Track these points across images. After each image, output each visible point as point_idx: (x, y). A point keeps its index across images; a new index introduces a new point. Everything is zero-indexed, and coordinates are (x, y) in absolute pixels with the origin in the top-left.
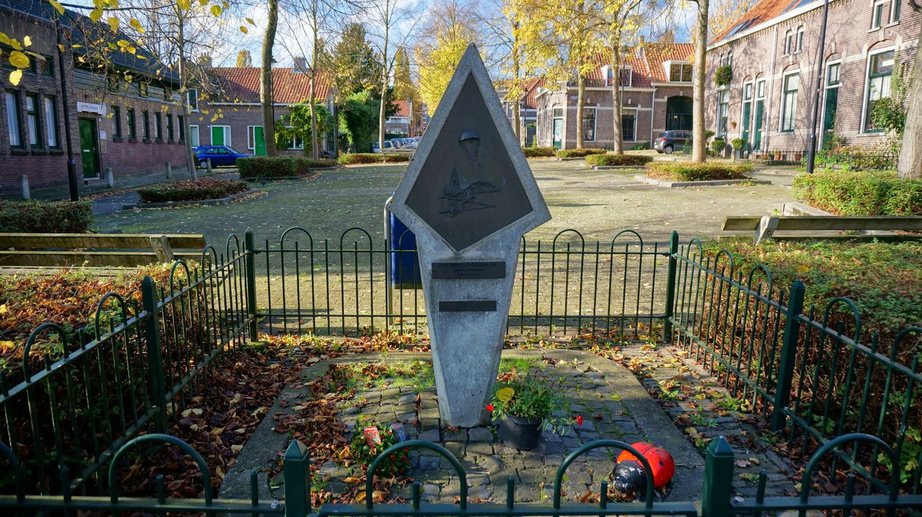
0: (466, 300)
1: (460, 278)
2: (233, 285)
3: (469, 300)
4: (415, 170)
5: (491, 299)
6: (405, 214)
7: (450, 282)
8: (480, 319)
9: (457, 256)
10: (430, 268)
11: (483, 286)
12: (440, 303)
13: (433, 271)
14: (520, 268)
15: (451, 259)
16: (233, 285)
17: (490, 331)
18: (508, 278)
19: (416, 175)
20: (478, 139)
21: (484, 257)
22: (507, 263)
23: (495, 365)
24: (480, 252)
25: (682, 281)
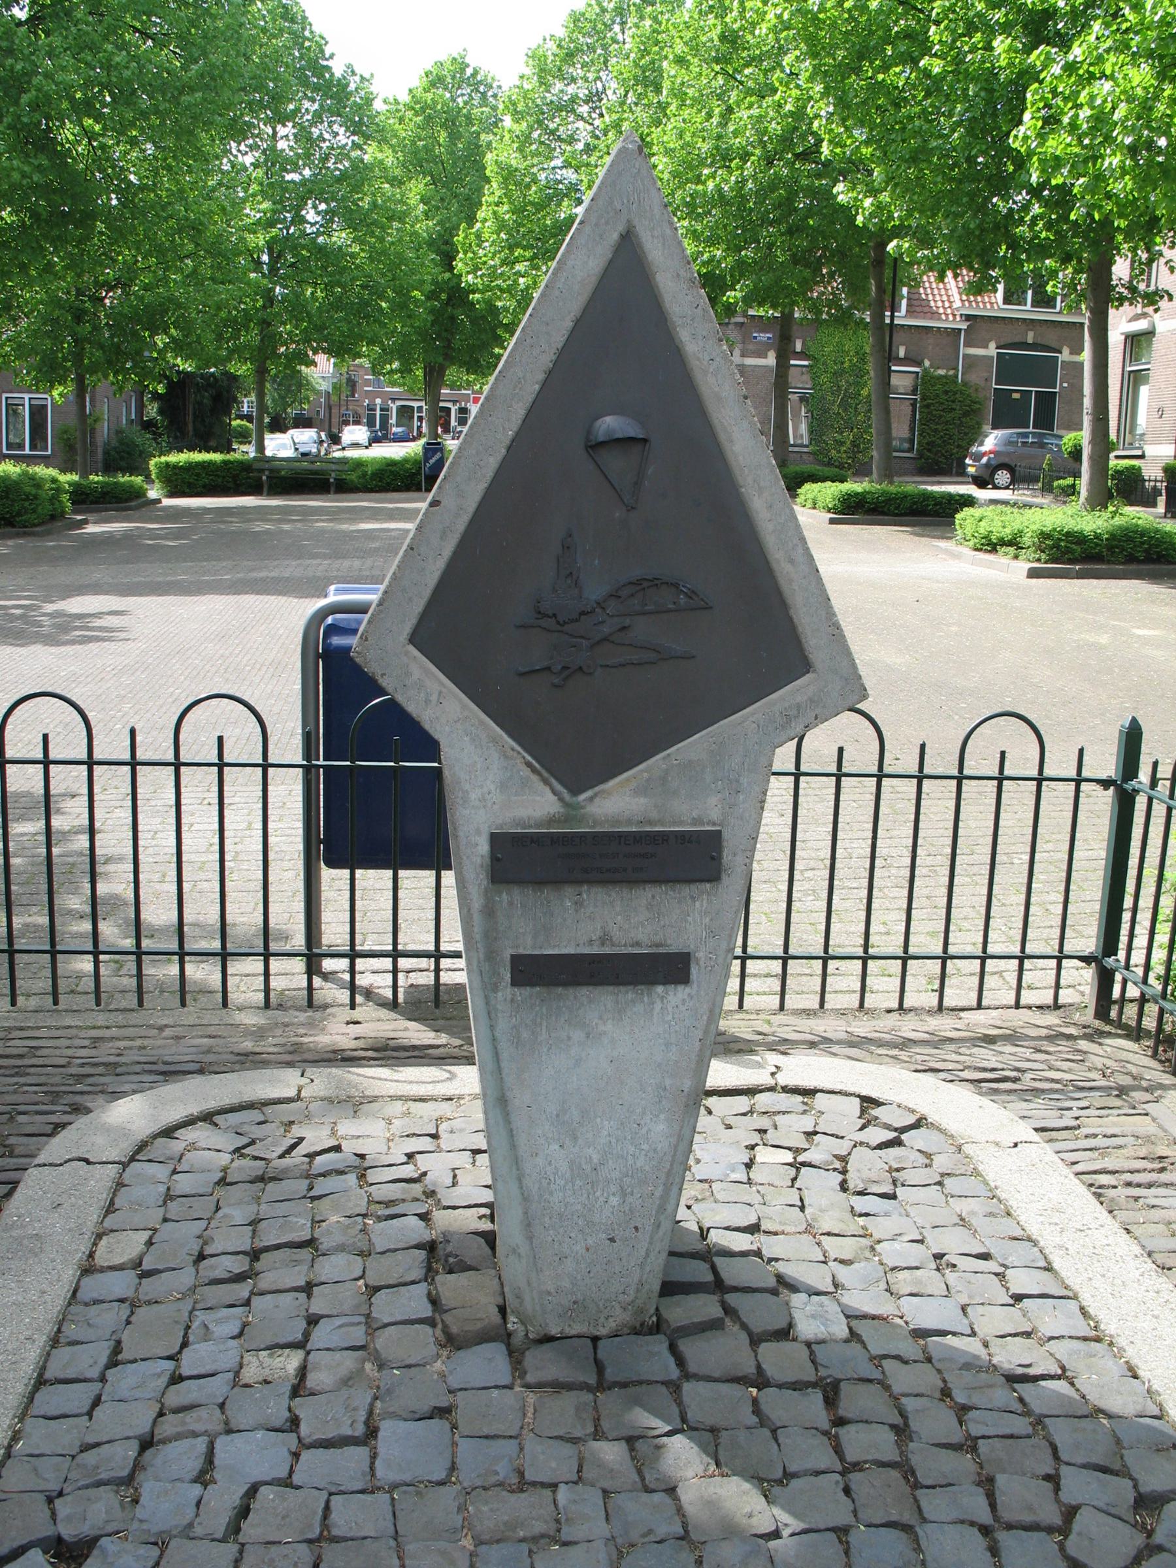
0: (595, 950)
1: (579, 882)
2: (931, 887)
3: (607, 950)
4: (443, 536)
5: (675, 947)
6: (408, 674)
7: (547, 891)
8: (639, 1008)
9: (571, 813)
10: (484, 847)
11: (649, 907)
12: (515, 959)
13: (494, 859)
14: (733, 984)
15: (551, 821)
16: (931, 887)
17: (668, 1045)
18: (731, 884)
19: (448, 551)
20: (645, 441)
21: (654, 815)
22: (726, 835)
23: (681, 1148)
24: (643, 800)
25: (1146, 902)
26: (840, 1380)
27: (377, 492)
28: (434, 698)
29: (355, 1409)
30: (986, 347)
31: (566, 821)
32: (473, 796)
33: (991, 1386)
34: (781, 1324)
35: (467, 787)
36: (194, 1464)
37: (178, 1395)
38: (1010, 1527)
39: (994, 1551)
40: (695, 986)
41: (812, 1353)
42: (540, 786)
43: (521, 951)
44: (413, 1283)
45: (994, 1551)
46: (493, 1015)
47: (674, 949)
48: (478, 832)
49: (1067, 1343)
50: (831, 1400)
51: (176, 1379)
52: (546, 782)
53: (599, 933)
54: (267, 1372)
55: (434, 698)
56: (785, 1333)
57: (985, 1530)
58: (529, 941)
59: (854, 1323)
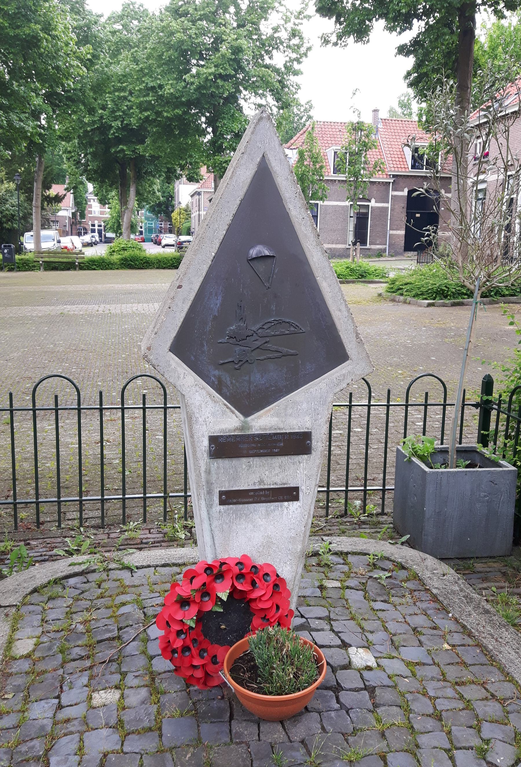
8: (277, 513)
11: (280, 466)
24: (276, 419)
26: (375, 687)
27: (62, 270)
28: (182, 376)
29: (150, 714)
30: (403, 191)
31: (242, 429)
32: (200, 419)
33: (445, 687)
34: (346, 662)
35: (198, 415)
36: (74, 746)
37: (62, 715)
38: (457, 749)
39: (452, 758)
40: (301, 502)
41: (361, 674)
42: (230, 414)
43: (223, 489)
44: (387, 414)
45: (452, 758)
46: (211, 519)
47: (292, 485)
48: (203, 436)
49: (477, 667)
50: (372, 695)
51: (60, 707)
52: (233, 412)
53: (258, 479)
54: (104, 700)
55: (182, 376)
56: (348, 666)
57: (448, 751)
58: (227, 485)
59: (379, 660)
